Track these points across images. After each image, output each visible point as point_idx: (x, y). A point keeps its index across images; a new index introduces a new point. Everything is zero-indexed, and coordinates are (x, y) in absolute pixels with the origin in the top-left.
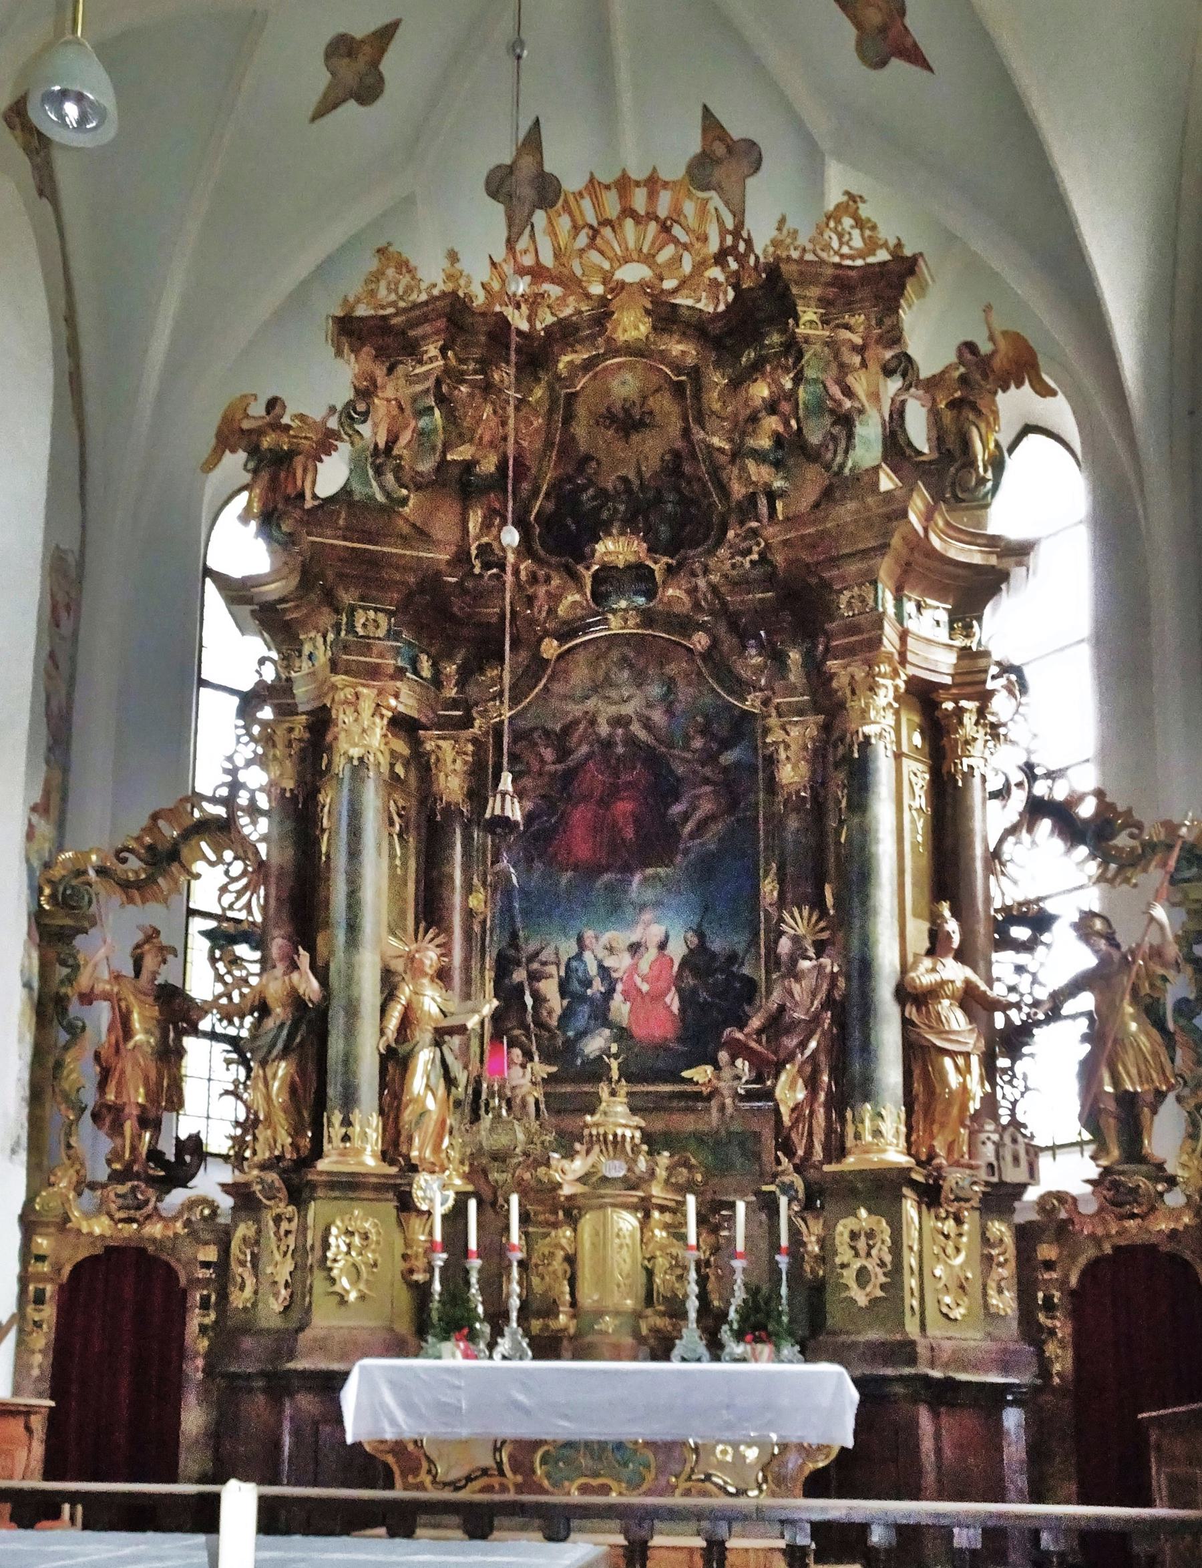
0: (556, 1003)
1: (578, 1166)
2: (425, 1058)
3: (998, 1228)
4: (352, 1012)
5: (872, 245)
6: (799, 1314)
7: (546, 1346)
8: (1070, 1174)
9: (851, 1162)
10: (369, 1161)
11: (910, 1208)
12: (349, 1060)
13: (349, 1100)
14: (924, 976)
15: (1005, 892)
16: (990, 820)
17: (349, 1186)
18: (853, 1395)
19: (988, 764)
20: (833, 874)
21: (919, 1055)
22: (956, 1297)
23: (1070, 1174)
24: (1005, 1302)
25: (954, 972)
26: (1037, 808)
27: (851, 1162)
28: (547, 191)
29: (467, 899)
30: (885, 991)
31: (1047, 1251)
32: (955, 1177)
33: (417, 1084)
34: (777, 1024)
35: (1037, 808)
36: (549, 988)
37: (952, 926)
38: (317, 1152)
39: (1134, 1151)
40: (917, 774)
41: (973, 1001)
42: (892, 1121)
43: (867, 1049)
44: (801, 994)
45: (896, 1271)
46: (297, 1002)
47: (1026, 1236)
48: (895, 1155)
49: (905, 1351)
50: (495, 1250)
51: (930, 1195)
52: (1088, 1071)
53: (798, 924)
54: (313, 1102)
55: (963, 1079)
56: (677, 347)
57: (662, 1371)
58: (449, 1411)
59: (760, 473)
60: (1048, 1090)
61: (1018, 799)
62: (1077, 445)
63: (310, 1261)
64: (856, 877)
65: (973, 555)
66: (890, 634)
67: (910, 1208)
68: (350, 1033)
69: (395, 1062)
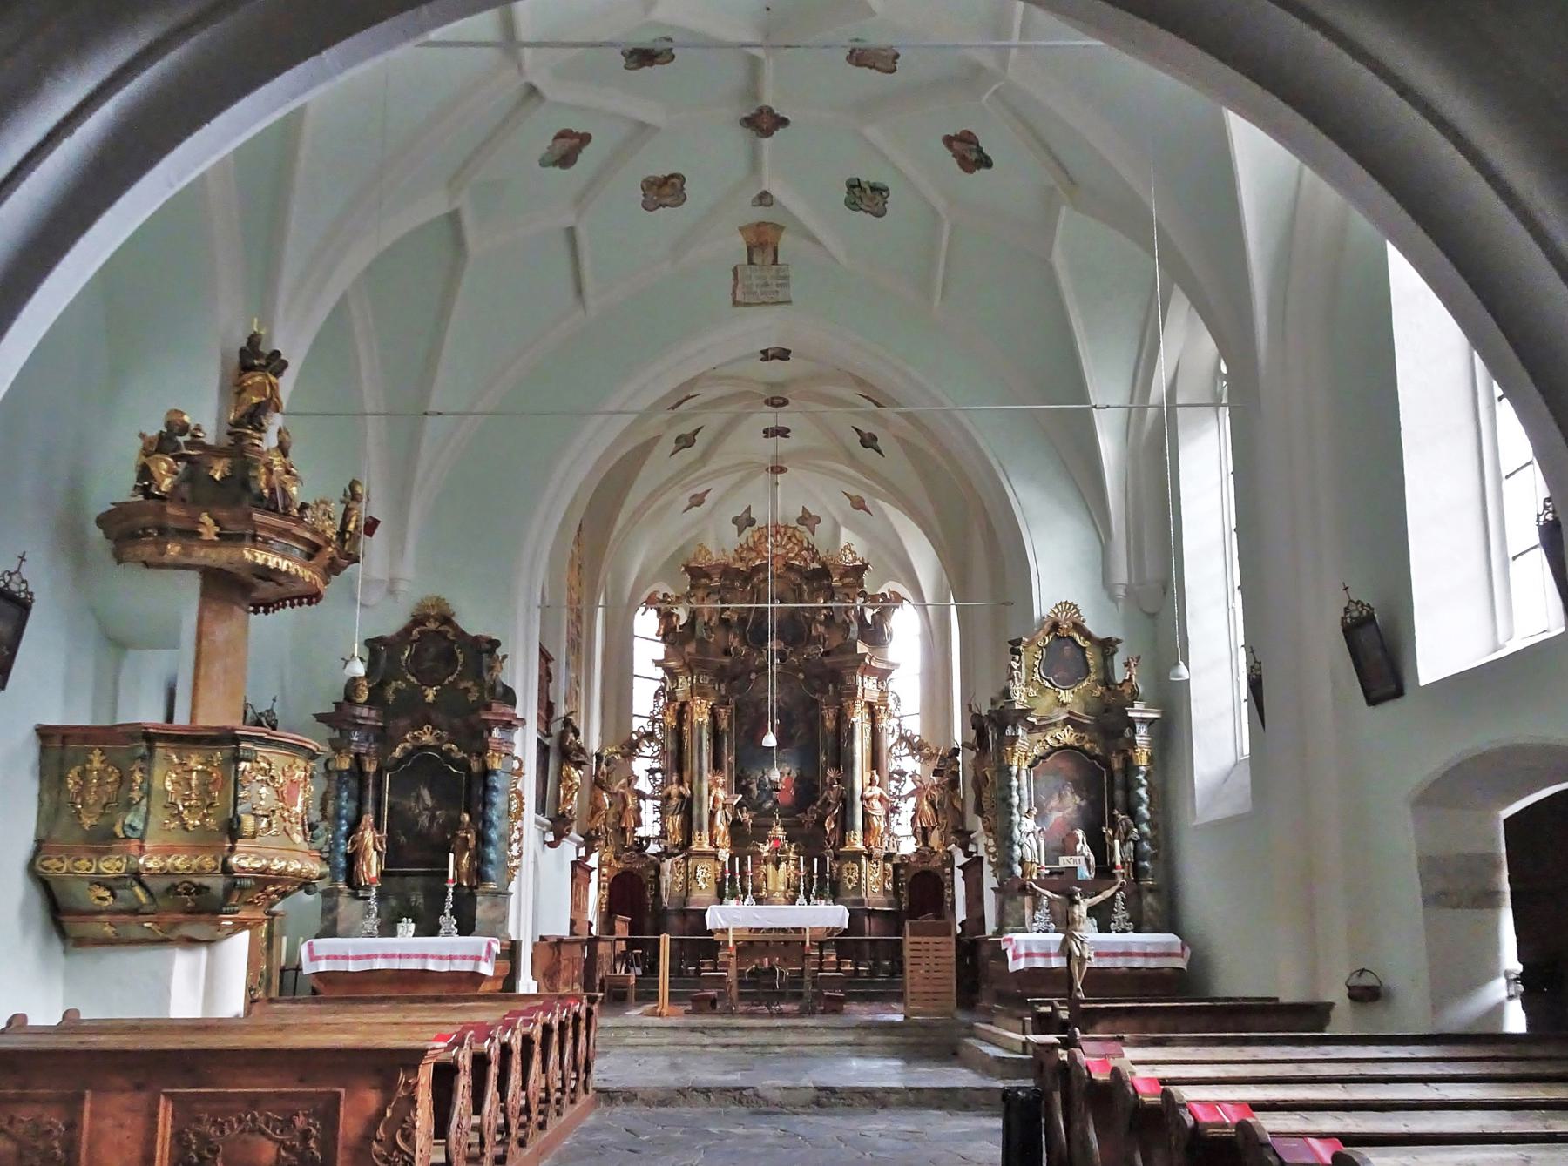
0: (756, 792)
1: (767, 847)
2: (719, 814)
3: (889, 865)
4: (700, 800)
5: (855, 559)
6: (832, 890)
7: (759, 901)
8: (908, 847)
9: (847, 848)
10: (706, 847)
11: (863, 861)
12: (700, 815)
13: (700, 828)
14: (867, 794)
15: (894, 765)
16: (889, 741)
17: (702, 854)
18: (847, 914)
19: (887, 724)
20: (842, 759)
21: (866, 816)
22: (873, 883)
23: (908, 847)
24: (889, 887)
25: (877, 791)
26: (902, 738)
27: (847, 848)
28: (751, 522)
29: (729, 759)
30: (857, 798)
31: (902, 871)
32: (876, 851)
33: (718, 821)
34: (826, 804)
35: (902, 738)
36: (754, 786)
37: (876, 777)
38: (690, 843)
39: (926, 844)
40: (868, 726)
41: (881, 799)
42: (859, 835)
43: (853, 815)
44: (832, 796)
45: (859, 879)
46: (681, 796)
47: (896, 867)
48: (860, 846)
49: (862, 902)
50: (743, 873)
51: (869, 857)
52: (913, 820)
53: (831, 773)
54: (687, 828)
55: (878, 823)
56: (792, 576)
57: (1531, 792)
58: (737, 920)
59: (821, 629)
60: (902, 825)
61: (896, 735)
62: (928, 599)
63: (689, 878)
64: (850, 765)
65: (884, 666)
66: (860, 690)
67: (863, 861)
68: (700, 808)
69: (712, 815)
